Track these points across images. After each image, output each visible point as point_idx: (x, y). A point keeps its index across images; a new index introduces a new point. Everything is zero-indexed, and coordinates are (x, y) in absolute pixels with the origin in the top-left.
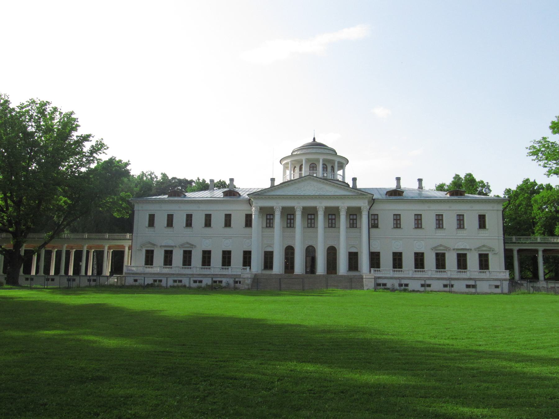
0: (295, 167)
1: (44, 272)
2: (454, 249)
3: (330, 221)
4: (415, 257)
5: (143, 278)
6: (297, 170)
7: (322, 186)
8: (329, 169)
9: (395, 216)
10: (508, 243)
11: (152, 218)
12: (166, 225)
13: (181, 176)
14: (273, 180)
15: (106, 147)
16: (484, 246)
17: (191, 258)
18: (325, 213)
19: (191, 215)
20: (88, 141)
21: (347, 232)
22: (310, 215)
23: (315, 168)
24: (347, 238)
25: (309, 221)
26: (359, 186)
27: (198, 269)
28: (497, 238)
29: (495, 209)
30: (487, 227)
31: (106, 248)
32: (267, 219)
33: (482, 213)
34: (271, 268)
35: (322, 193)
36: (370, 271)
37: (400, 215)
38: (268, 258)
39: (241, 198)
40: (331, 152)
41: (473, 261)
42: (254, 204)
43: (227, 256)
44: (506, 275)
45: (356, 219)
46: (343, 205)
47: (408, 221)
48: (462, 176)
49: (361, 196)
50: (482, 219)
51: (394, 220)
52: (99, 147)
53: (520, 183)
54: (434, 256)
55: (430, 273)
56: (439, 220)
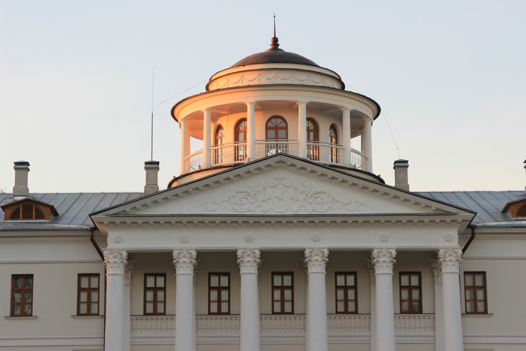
9: (469, 278)
14: (152, 166)
21: (329, 328)
23: (281, 133)
42: (111, 244)
46: (385, 244)
49: (438, 219)
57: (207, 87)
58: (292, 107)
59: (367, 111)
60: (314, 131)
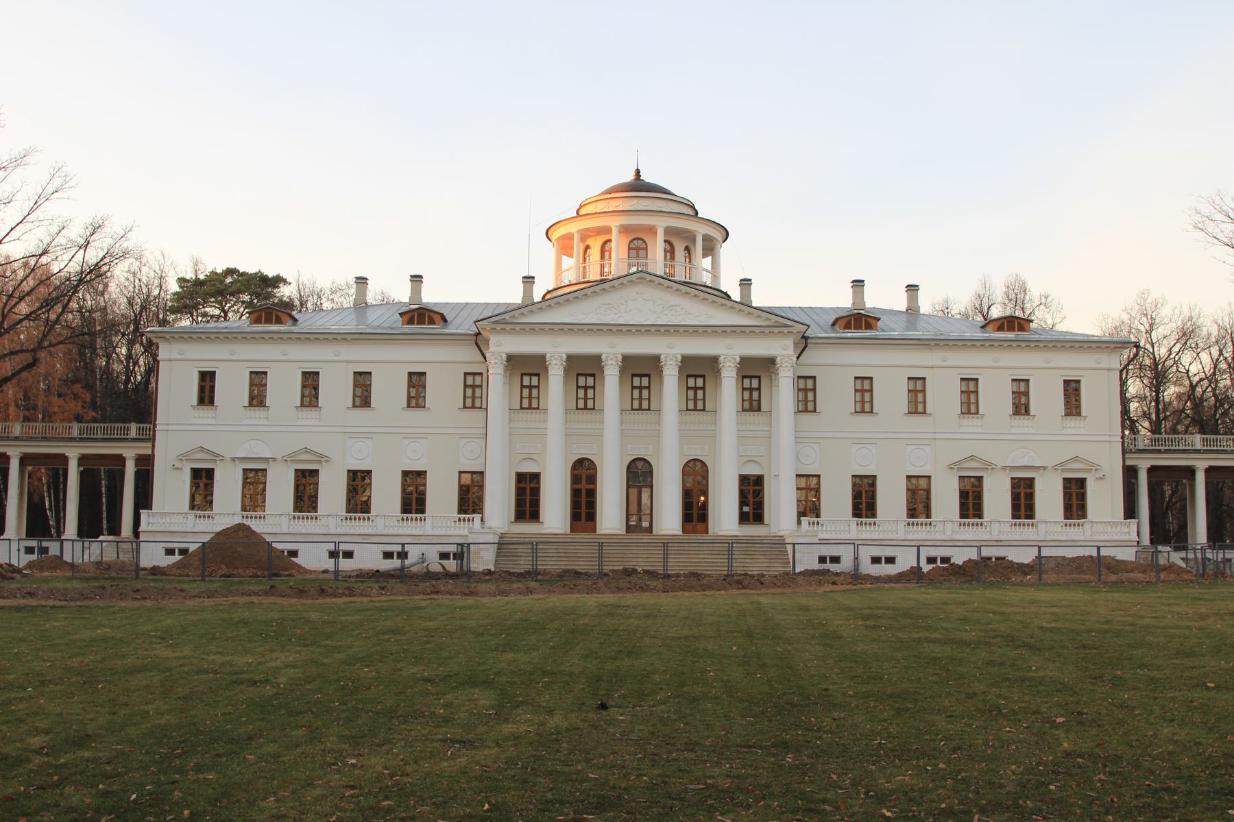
0: (587, 247)
2: (1004, 468)
8: (680, 253)
10: (1130, 451)
11: (207, 382)
14: (529, 280)
16: (1076, 459)
19: (213, 374)
22: (641, 373)
24: (741, 438)
25: (581, 392)
26: (759, 298)
27: (285, 520)
28: (1107, 438)
29: (1102, 366)
30: (1083, 413)
36: (799, 523)
43: (1022, 491)
45: (759, 389)
46: (730, 352)
47: (891, 394)
50: (1072, 390)
51: (856, 391)
55: (996, 527)
56: (970, 390)
57: (578, 212)
58: (652, 230)
59: (717, 235)
60: (670, 252)
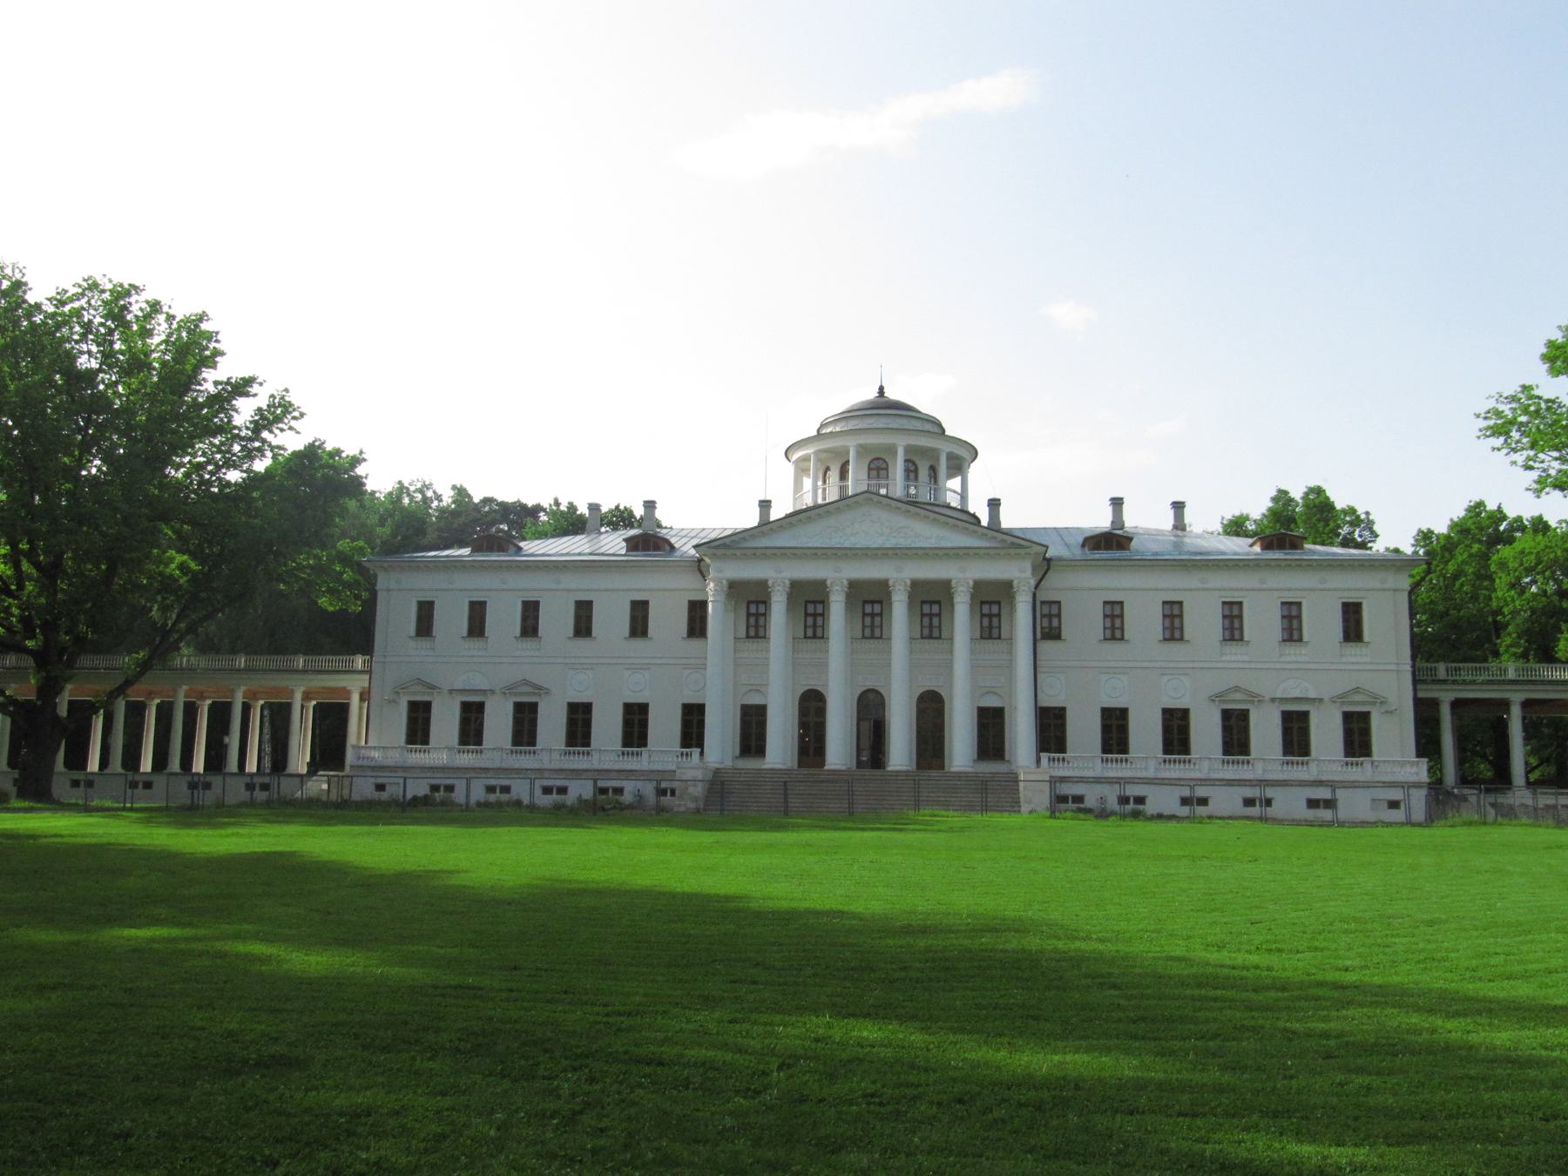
0: (828, 469)
1: (125, 765)
2: (1273, 700)
3: (926, 620)
4: (1164, 720)
5: (401, 781)
6: (834, 476)
7: (902, 521)
8: (924, 474)
9: (1108, 607)
10: (1424, 682)
11: (426, 612)
12: (465, 632)
13: (507, 495)
14: (765, 505)
15: (296, 414)
16: (1357, 690)
17: (535, 725)
18: (912, 597)
19: (537, 604)
20: (247, 395)
21: (972, 652)
22: (869, 602)
23: (883, 473)
24: (974, 668)
25: (868, 620)
26: (1008, 521)
27: (556, 756)
28: (1394, 667)
29: (1387, 586)
30: (1366, 637)
31: (298, 697)
32: (749, 615)
33: (1352, 598)
34: (760, 751)
35: (904, 543)
36: (1038, 761)
37: (1121, 603)
38: (753, 725)
39: (676, 556)
40: (928, 427)
41: (1326, 733)
42: (712, 574)
43: (636, 718)
44: (1419, 771)
45: (999, 615)
46: (963, 576)
47: (1144, 620)
48: (1297, 494)
49: (1012, 551)
50: (1352, 616)
51: (1105, 616)
52: (277, 413)
53: (1459, 512)
54: (1217, 719)
55: (1205, 765)
56: (1233, 616)
